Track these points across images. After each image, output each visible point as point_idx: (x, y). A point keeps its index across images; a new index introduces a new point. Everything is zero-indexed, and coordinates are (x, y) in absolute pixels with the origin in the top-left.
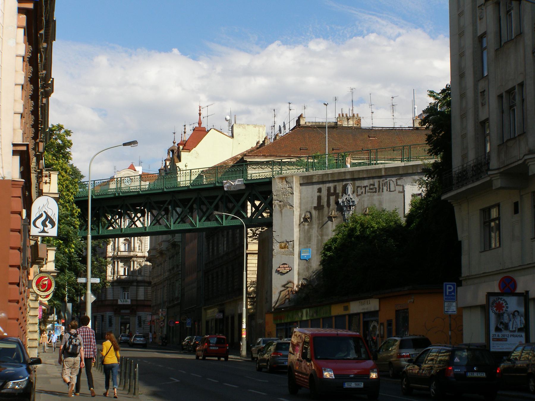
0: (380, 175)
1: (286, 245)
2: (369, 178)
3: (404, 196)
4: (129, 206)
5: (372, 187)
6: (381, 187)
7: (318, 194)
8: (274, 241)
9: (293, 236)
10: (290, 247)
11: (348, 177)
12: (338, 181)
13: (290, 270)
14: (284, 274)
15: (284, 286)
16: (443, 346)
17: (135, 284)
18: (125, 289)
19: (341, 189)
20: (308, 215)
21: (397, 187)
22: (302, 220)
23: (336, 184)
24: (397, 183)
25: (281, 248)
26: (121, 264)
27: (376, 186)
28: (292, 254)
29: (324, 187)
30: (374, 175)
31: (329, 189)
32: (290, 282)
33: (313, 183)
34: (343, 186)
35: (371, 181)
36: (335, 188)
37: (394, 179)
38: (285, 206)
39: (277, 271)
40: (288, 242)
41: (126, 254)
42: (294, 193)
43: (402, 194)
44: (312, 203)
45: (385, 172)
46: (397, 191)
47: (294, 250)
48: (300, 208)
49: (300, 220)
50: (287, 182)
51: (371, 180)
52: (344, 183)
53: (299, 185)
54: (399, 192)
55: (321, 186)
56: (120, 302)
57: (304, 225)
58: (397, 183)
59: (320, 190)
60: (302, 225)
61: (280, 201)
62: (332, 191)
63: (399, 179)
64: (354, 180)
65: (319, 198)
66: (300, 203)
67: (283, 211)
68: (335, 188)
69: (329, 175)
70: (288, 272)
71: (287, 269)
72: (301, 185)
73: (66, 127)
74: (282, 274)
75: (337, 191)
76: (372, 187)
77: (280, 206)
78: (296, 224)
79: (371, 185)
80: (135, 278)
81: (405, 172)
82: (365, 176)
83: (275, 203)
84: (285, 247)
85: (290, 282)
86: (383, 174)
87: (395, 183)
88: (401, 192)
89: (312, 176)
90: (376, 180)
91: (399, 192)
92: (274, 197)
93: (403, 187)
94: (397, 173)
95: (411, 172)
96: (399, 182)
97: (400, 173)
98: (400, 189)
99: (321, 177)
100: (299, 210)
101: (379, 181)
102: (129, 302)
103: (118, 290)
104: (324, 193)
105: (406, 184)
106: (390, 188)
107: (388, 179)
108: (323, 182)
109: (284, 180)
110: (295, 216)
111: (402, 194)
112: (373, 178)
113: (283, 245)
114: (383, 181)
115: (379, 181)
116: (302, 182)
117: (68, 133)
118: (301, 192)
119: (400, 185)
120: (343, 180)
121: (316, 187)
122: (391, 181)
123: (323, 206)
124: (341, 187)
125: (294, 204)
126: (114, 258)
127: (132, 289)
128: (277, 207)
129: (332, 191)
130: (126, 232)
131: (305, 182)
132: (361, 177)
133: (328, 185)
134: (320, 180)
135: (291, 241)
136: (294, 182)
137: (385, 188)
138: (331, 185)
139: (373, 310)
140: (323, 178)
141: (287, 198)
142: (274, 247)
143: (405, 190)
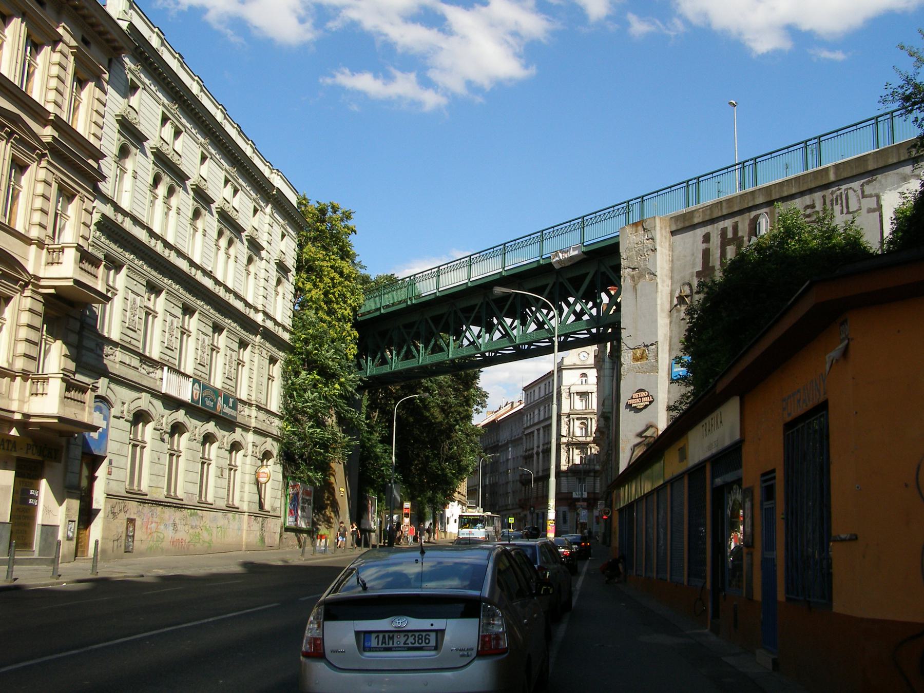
0: (824, 182)
1: (645, 352)
2: (802, 194)
3: (881, 216)
4: (430, 321)
5: (808, 211)
6: (828, 207)
7: (704, 246)
8: (623, 347)
9: (656, 334)
10: (651, 355)
11: (760, 200)
12: (741, 212)
13: (651, 402)
14: (641, 410)
15: (640, 435)
16: (621, 530)
17: (592, 474)
18: (580, 480)
19: (747, 229)
20: (687, 290)
21: (864, 201)
22: (675, 302)
23: (736, 219)
24: (863, 192)
25: (636, 359)
26: (576, 451)
27: (819, 207)
28: (655, 369)
29: (714, 230)
30: (813, 186)
31: (724, 232)
32: (651, 426)
33: (693, 227)
34: (751, 220)
35: (807, 200)
36: (735, 228)
37: (856, 185)
38: (641, 276)
39: (629, 406)
40: (647, 346)
41: (583, 439)
42: (658, 248)
43: (877, 213)
44: (694, 265)
45: (836, 174)
46: (864, 210)
47: (657, 361)
48: (672, 278)
49: (671, 302)
50: (644, 229)
51: (807, 197)
52: (753, 214)
53: (669, 235)
54: (870, 211)
55: (708, 229)
56: (574, 495)
57: (679, 311)
58: (863, 192)
59: (707, 238)
60: (674, 311)
61: (634, 269)
62: (730, 235)
63: (868, 183)
64: (770, 203)
65: (706, 253)
66: (672, 270)
67: (639, 287)
68: (735, 228)
69: (724, 204)
70: (646, 406)
71: (646, 401)
72: (673, 233)
73: (344, 207)
74: (637, 410)
75: (740, 234)
76: (808, 211)
77: (633, 277)
78: (662, 310)
79: (807, 207)
80: (592, 467)
81: (880, 165)
82: (794, 191)
83: (625, 272)
84: (642, 358)
85: (651, 426)
86: (832, 177)
87: (859, 192)
88: (874, 210)
89: (692, 213)
90: (818, 196)
91: (870, 211)
92: (624, 263)
93: (878, 197)
94: (862, 171)
95: (895, 161)
96: (868, 190)
97: (870, 168)
98: (871, 203)
99: (708, 212)
100: (669, 282)
101: (824, 197)
102: (585, 495)
103: (574, 480)
104: (716, 240)
105: (884, 189)
106: (848, 207)
107: (844, 187)
108: (713, 221)
109: (640, 228)
110: (659, 294)
111: (877, 213)
112: (811, 191)
113: (639, 352)
114: (832, 193)
115: (824, 197)
116: (674, 228)
117: (347, 216)
118: (672, 248)
119: (871, 196)
120: (750, 209)
121: (700, 232)
122: (850, 192)
123: (713, 267)
124: (747, 222)
125: (658, 270)
126: (568, 444)
127: (589, 480)
128: (629, 280)
129: (730, 235)
130: (424, 363)
131: (680, 226)
132: (785, 194)
133: (721, 225)
134: (707, 218)
135: (652, 345)
136: (658, 228)
137: (837, 208)
138: (728, 223)
139: (727, 443)
140: (712, 212)
141: (645, 260)
142: (622, 360)
143: (883, 203)
